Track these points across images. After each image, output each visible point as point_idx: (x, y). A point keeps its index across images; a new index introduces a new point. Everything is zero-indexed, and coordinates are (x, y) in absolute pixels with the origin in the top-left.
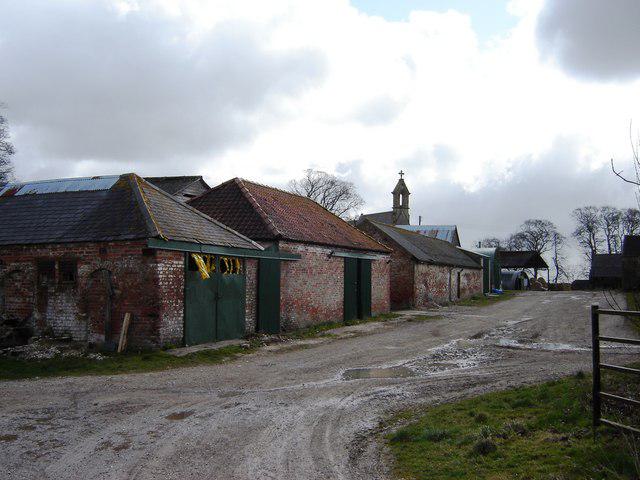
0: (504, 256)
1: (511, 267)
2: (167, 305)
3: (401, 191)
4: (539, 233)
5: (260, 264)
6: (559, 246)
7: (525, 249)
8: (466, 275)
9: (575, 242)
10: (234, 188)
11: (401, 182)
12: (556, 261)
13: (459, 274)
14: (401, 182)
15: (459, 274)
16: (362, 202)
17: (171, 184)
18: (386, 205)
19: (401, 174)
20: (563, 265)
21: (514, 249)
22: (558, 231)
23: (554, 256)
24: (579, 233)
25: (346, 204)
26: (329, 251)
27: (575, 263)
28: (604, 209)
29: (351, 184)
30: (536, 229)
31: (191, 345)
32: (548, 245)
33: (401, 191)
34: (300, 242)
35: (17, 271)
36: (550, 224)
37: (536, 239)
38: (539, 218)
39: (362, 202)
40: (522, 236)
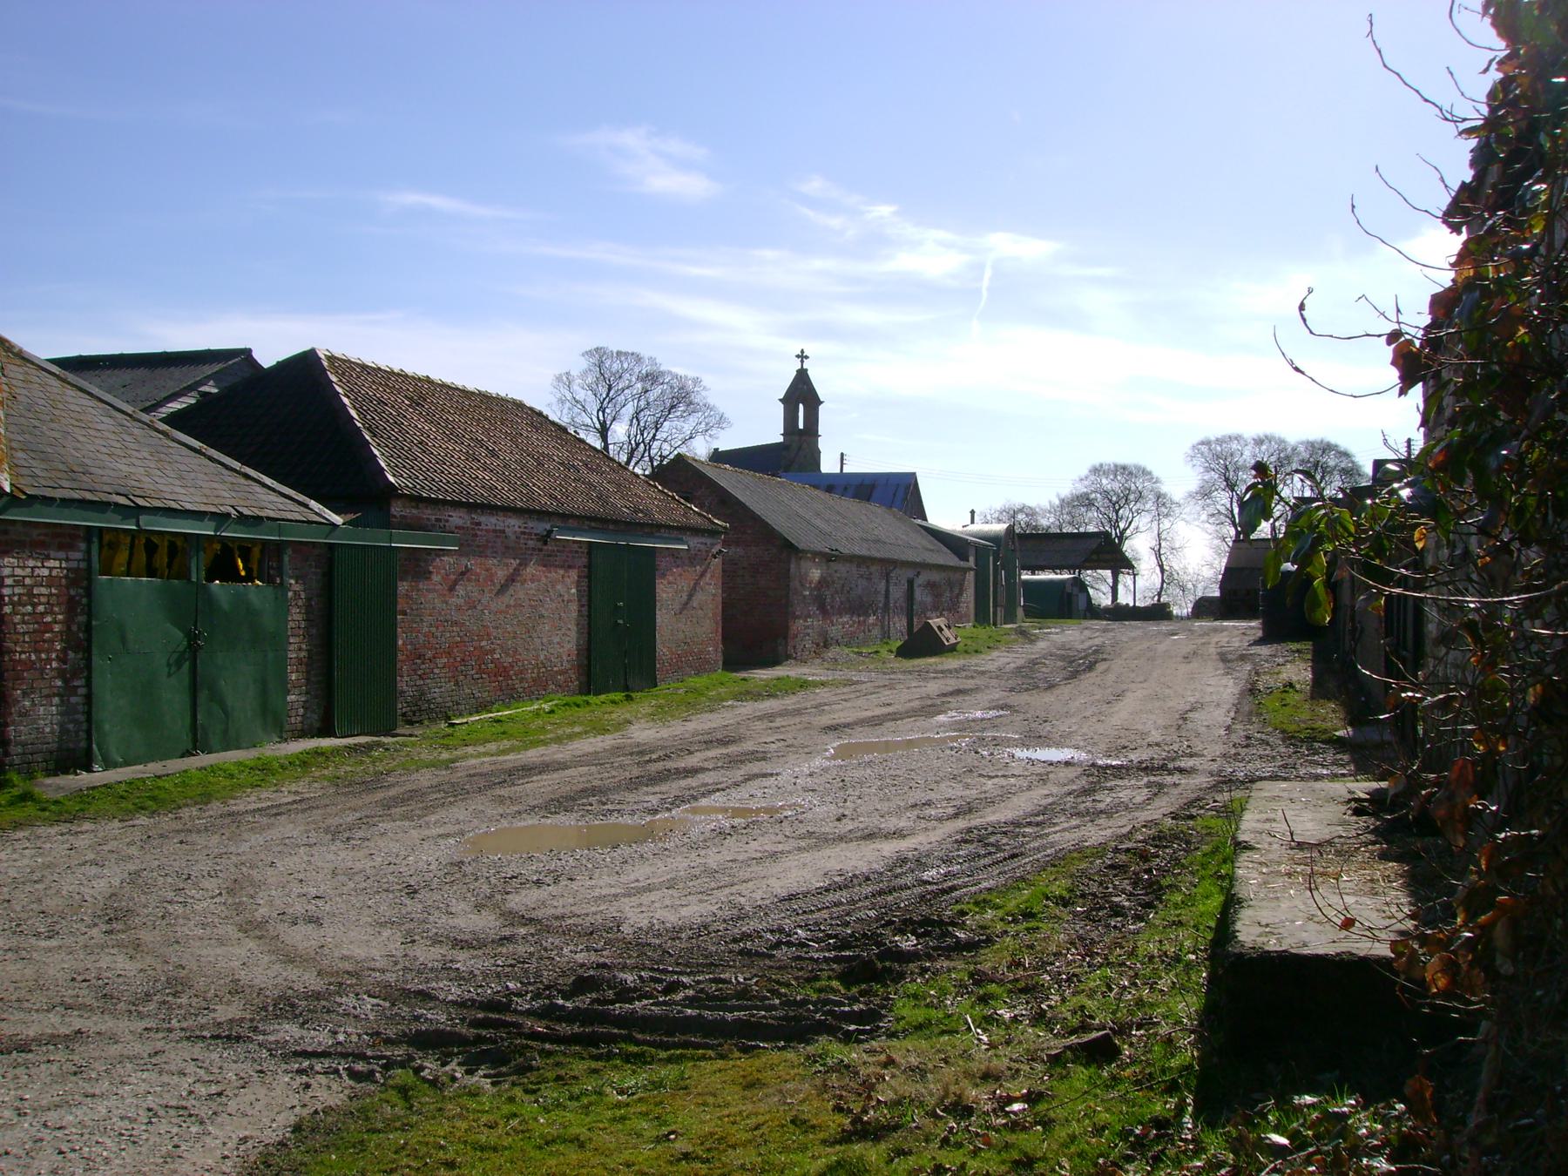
0: (1025, 543)
1: (1048, 570)
2: (30, 665)
3: (802, 395)
4: (1124, 489)
5: (328, 560)
6: (1166, 524)
7: (1091, 529)
8: (931, 586)
9: (1191, 509)
10: (305, 370)
11: (802, 378)
12: (1158, 555)
13: (911, 583)
14: (802, 378)
15: (911, 583)
16: (721, 421)
17: (718, 457)
18: (770, 431)
19: (802, 356)
20: (1174, 563)
21: (1067, 529)
22: (1164, 489)
23: (1154, 543)
24: (1205, 493)
25: (687, 428)
26: (541, 527)
27: (1187, 549)
28: (1259, 442)
29: (696, 381)
30: (1116, 486)
31: (109, 764)
32: (1142, 521)
33: (802, 395)
34: (456, 504)
35: (1332, 563)
36: (1145, 473)
37: (1116, 507)
38: (1122, 461)
39: (721, 421)
40: (1085, 501)
